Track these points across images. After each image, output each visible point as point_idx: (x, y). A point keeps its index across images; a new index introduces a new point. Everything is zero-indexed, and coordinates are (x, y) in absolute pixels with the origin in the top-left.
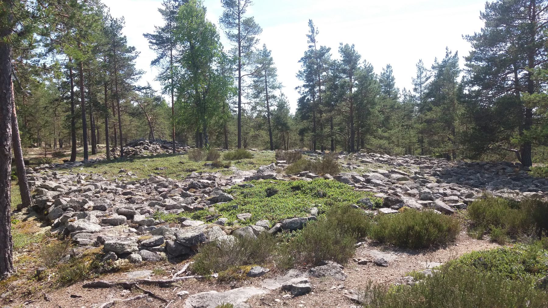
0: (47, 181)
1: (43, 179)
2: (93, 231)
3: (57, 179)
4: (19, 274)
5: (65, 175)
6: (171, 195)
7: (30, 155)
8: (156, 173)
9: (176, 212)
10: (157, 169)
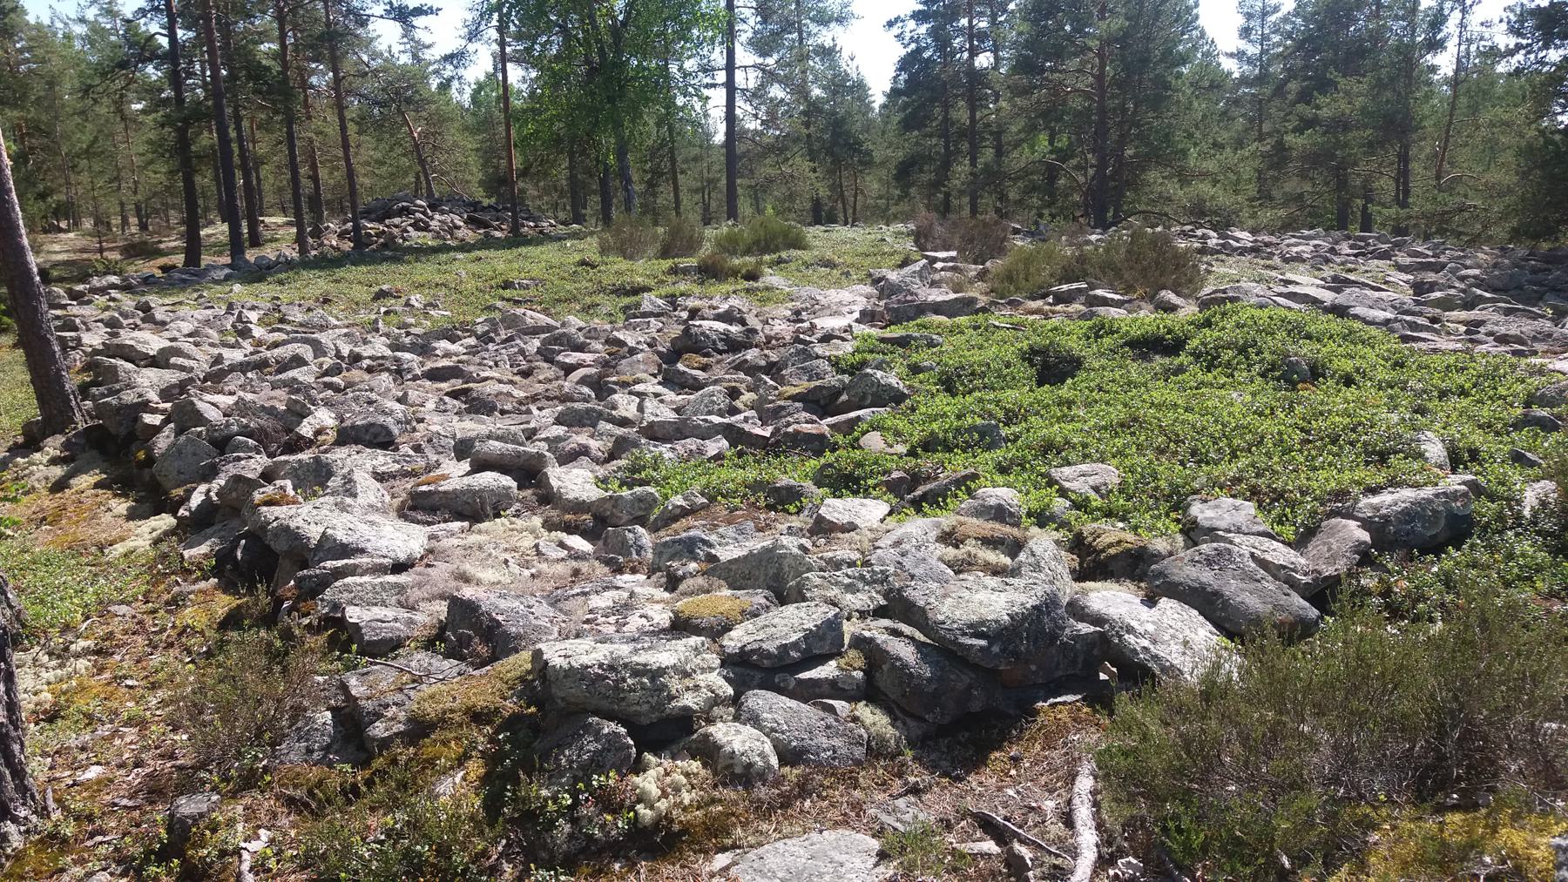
0: (122, 332)
1: (107, 325)
2: (402, 557)
3: (156, 323)
4: (69, 830)
5: (183, 311)
6: (624, 378)
7: (49, 252)
8: (508, 300)
9: (700, 452)
10: (507, 285)
